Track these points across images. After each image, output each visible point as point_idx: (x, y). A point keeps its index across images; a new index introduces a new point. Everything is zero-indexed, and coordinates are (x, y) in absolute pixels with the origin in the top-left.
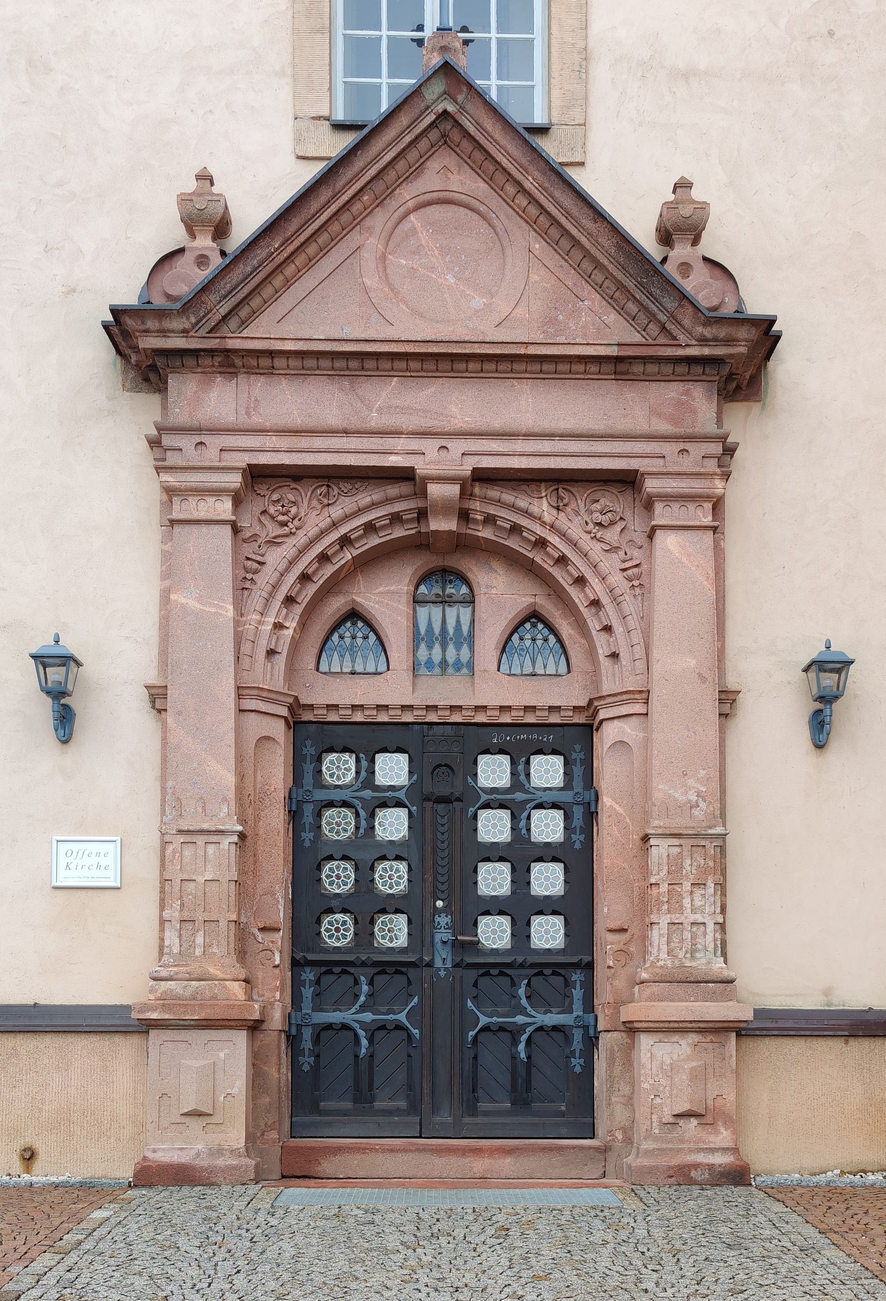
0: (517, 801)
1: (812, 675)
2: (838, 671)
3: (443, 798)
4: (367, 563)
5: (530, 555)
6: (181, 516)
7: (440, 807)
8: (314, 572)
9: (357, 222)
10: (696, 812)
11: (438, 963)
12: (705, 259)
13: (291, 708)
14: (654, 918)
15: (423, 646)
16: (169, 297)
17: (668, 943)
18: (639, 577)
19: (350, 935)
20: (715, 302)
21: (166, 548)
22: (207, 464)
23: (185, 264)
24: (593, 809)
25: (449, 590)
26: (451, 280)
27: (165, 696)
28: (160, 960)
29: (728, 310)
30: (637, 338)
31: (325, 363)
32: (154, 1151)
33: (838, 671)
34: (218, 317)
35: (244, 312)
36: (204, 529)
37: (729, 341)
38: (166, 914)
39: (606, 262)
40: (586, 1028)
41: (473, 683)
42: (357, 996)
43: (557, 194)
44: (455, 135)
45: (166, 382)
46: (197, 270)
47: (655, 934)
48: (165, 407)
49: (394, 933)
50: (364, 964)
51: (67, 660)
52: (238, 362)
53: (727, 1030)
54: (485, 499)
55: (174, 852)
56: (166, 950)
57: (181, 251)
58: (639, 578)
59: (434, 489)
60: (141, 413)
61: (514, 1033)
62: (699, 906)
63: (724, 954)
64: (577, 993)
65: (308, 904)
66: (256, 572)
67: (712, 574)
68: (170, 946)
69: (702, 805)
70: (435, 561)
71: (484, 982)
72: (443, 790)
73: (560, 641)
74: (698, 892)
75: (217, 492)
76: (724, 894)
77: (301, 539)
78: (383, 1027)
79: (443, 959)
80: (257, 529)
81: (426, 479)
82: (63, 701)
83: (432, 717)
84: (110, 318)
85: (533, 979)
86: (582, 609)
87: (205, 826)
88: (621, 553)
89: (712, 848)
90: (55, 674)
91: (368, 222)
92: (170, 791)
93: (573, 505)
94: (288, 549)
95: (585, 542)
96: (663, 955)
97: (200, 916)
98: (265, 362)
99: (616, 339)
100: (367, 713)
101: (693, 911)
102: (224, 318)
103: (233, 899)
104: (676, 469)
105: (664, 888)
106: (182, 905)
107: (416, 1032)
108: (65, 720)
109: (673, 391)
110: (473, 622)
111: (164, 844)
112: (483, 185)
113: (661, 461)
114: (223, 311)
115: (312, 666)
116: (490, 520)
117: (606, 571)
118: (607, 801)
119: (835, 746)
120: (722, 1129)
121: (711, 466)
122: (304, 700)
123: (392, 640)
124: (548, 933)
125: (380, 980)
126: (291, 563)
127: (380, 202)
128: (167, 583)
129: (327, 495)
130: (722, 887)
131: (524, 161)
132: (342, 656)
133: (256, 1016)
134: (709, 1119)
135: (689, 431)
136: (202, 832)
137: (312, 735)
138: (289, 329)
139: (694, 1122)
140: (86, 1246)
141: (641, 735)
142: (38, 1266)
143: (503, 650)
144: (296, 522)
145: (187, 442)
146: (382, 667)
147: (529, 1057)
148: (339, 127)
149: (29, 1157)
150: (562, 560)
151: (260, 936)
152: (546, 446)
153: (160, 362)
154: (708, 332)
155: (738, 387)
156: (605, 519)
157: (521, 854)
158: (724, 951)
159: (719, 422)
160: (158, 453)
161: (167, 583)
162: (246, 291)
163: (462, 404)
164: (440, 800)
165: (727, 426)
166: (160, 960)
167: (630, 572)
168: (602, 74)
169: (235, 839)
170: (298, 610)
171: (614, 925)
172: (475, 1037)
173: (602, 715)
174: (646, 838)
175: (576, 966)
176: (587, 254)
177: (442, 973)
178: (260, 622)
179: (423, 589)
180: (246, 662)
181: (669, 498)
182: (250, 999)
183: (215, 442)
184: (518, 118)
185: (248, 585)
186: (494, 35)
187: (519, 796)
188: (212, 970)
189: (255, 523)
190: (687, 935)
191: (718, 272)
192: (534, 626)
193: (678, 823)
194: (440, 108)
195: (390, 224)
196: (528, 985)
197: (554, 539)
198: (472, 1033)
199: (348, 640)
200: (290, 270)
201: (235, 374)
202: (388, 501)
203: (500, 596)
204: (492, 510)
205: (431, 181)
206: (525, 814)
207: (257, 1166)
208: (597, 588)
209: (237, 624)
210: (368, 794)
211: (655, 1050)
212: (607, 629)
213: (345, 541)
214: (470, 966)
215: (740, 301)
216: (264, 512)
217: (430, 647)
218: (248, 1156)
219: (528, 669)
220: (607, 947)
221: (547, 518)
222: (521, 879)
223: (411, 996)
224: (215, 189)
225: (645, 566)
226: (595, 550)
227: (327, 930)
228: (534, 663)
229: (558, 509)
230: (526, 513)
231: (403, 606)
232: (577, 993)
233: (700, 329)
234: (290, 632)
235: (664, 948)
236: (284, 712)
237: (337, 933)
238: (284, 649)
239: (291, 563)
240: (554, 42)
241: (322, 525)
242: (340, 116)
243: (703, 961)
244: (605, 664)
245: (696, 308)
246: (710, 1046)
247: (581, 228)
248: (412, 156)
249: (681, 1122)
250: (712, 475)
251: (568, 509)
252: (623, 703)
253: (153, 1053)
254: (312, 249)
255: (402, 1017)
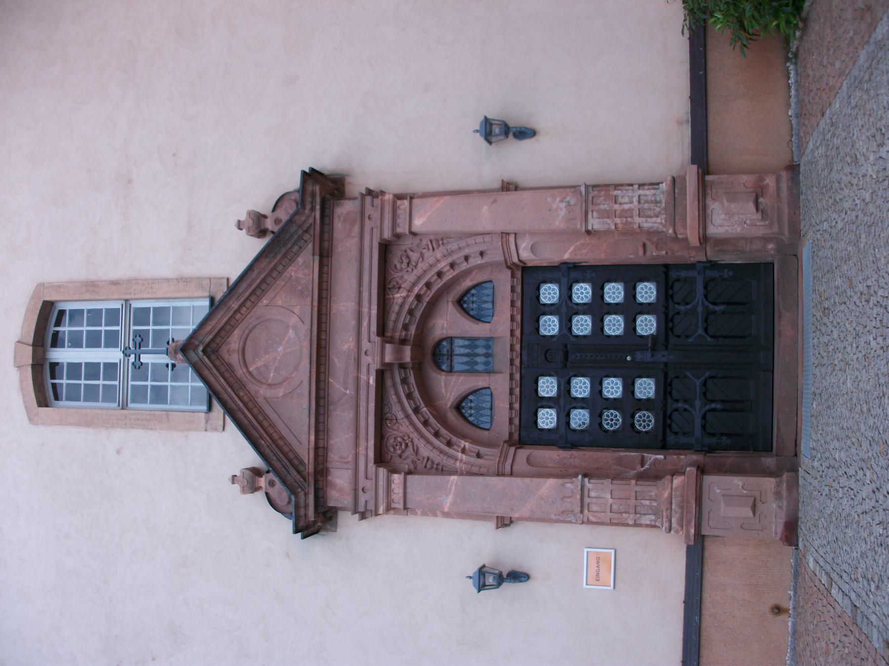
0: (566, 310)
1: (493, 139)
2: (491, 125)
3: (566, 357)
4: (429, 397)
5: (425, 304)
6: (402, 503)
7: (571, 357)
8: (434, 429)
9: (253, 399)
10: (572, 202)
11: (665, 359)
12: (274, 210)
13: (511, 445)
14: (636, 226)
15: (476, 367)
16: (289, 502)
17: (651, 217)
18: (437, 241)
19: (647, 413)
20: (294, 204)
21: (419, 512)
22: (374, 486)
23: (273, 493)
24: (571, 266)
25: (445, 351)
26: (280, 349)
27: (503, 518)
28: (658, 527)
29: (297, 196)
30: (310, 246)
31: (321, 419)
32: (776, 533)
33: (491, 125)
34: (298, 476)
35: (296, 462)
36: (409, 490)
37: (313, 195)
38: (631, 522)
39: (273, 264)
40: (705, 268)
41: (498, 338)
42: (685, 410)
43: (241, 291)
44: (214, 345)
45: (331, 507)
46: (276, 486)
47: (646, 225)
48: (344, 509)
49: (645, 388)
50: (665, 405)
51: (482, 572)
52: (321, 467)
53: (703, 180)
54: (394, 330)
55: (594, 516)
56: (653, 523)
57: (267, 494)
58: (438, 240)
59: (388, 359)
60: (348, 521)
61: (708, 314)
62: (628, 200)
63: (658, 184)
64: (683, 274)
65: (628, 439)
66: (433, 462)
67: (436, 199)
68: (651, 521)
69: (568, 199)
70: (428, 359)
71: (677, 331)
72: (560, 357)
73: (474, 287)
74: (620, 200)
75: (389, 482)
76: (622, 185)
77: (415, 436)
78: (705, 394)
79: (662, 356)
80: (409, 461)
81: (383, 363)
82: (505, 576)
83: (517, 362)
84: (299, 535)
85: (676, 300)
86: (455, 273)
87: (579, 497)
88: (424, 251)
89: (594, 193)
90: (490, 580)
91: (253, 394)
92: (558, 517)
93: (398, 279)
94: (420, 444)
95: (418, 271)
96: (659, 220)
97: (633, 502)
98: (321, 451)
99: (311, 257)
100: (514, 400)
101: (632, 202)
102: (299, 472)
103: (620, 482)
104: (379, 221)
105: (618, 220)
106: (626, 513)
107: (707, 374)
108: (517, 576)
109: (338, 225)
110: (462, 338)
111: (589, 522)
112: (236, 332)
113: (375, 230)
114: (295, 473)
115: (487, 433)
116: (406, 327)
117: (434, 261)
118: (566, 257)
119: (533, 124)
120: (765, 182)
121: (377, 202)
122: (506, 437)
123: (472, 385)
124: (647, 292)
125: (675, 395)
126: (428, 442)
127: (243, 386)
128: (439, 513)
129: (391, 420)
130: (617, 186)
131: (225, 309)
132: (482, 415)
133: (694, 469)
134: (759, 190)
135: (359, 215)
136: (582, 499)
137: (527, 435)
138: (304, 438)
139: (761, 200)
140: (828, 568)
141: (527, 236)
142: (839, 597)
143: (479, 320)
144: (406, 438)
145: (362, 498)
146: (488, 392)
147: (724, 303)
148: (210, 408)
149: (778, 610)
150: (428, 285)
151: (646, 466)
152: (365, 295)
153: (321, 510)
154: (308, 207)
155: (337, 189)
156: (405, 261)
157: (598, 309)
158: (655, 185)
159: (355, 199)
160: (368, 514)
161: (439, 513)
162: (285, 460)
163: (343, 343)
164: (566, 358)
165: (357, 194)
166: (658, 527)
167: (435, 246)
168: (189, 270)
169: (586, 480)
170: (454, 439)
171: (641, 252)
172: (712, 337)
173: (516, 260)
174: (588, 232)
175: (666, 274)
176: (269, 274)
177: (671, 357)
178: (461, 461)
179: (444, 367)
180: (483, 470)
181: (394, 224)
182: (684, 473)
183: (362, 482)
184: (206, 311)
185: (440, 467)
186: (85, 328)
187: (564, 310)
188: (666, 495)
189: (406, 462)
190: (646, 206)
191: (279, 204)
192: (465, 302)
193: (578, 212)
194: (201, 353)
195: (254, 381)
196: (678, 304)
197: (416, 290)
198: (709, 339)
199: (473, 412)
200: (276, 436)
201: (327, 469)
202: (394, 386)
203: (448, 322)
204: (400, 326)
205: (234, 359)
206: (575, 307)
207: (788, 471)
208: (443, 265)
209: (462, 474)
210: (562, 401)
211: (716, 224)
212: (466, 258)
213: (416, 410)
214: (667, 339)
215: (295, 191)
216: (400, 456)
217: (477, 363)
218: (781, 476)
219: (490, 306)
220: (655, 255)
221: (404, 294)
222: (614, 309)
223: (685, 377)
224: (238, 474)
225: (432, 237)
226: (422, 266)
227: (644, 427)
228: (486, 302)
229: (399, 288)
230: (402, 306)
231: (453, 378)
232: (683, 274)
233: (307, 211)
234: (467, 444)
235: (654, 219)
236: (512, 449)
237: (645, 421)
238: (476, 448)
239: (428, 442)
240: (174, 296)
241: (407, 423)
242: (205, 408)
243: (662, 196)
244: (486, 259)
245: (296, 213)
246: (714, 191)
247: (257, 276)
248: (223, 369)
249: (761, 207)
250: (382, 200)
251: (400, 282)
252: (509, 248)
253: (715, 532)
254: (266, 424)
255: (698, 382)
